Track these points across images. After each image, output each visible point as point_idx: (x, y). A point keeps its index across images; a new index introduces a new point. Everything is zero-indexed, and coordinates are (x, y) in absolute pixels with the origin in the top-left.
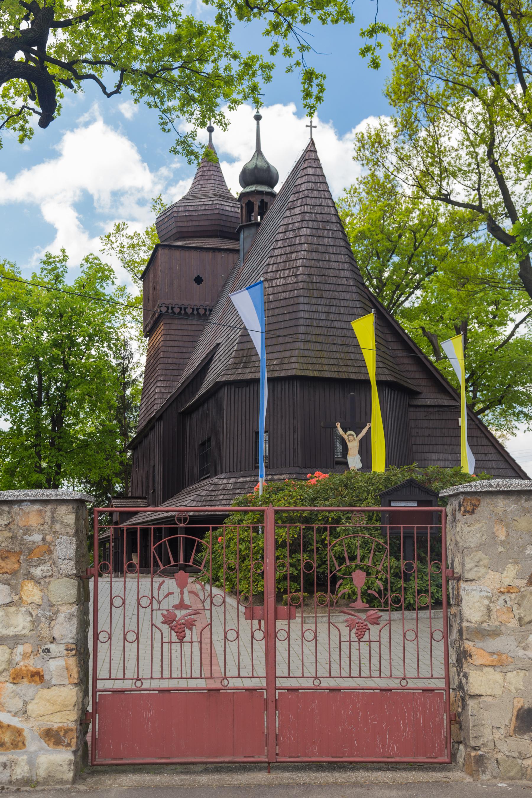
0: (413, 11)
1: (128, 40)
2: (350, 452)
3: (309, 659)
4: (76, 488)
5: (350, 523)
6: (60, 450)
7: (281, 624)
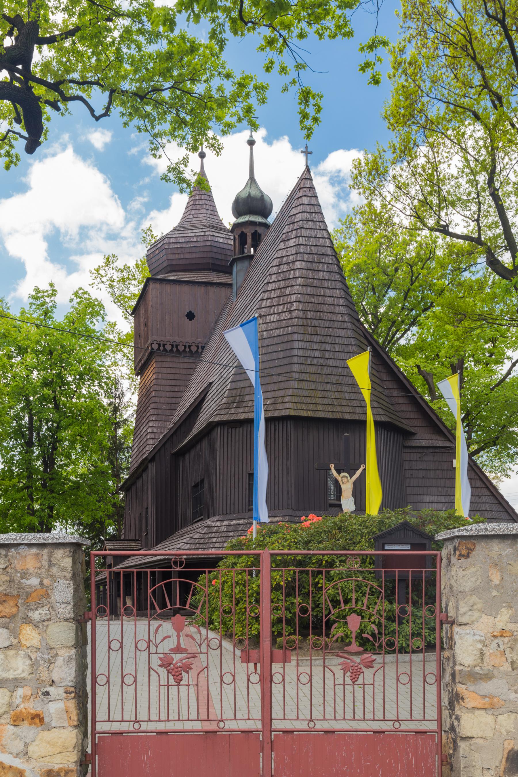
0: (414, 26)
1: (117, 58)
2: (344, 494)
3: (304, 701)
4: (68, 531)
5: (344, 566)
6: (52, 492)
7: (277, 668)
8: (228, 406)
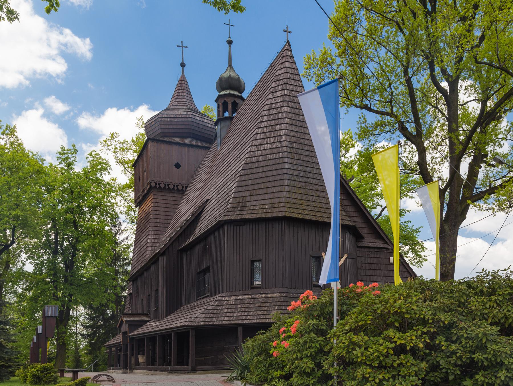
6: (71, 284)
8: (234, 209)
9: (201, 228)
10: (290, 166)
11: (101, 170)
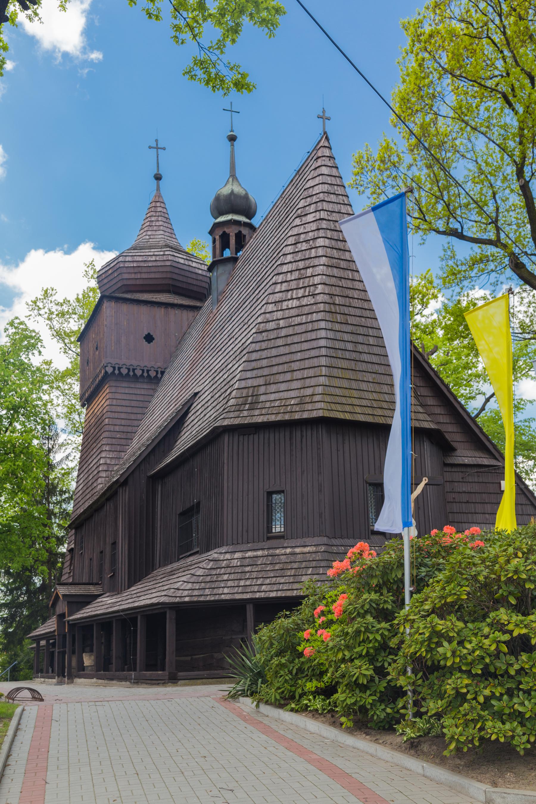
8: (239, 408)
9: (186, 439)
10: (330, 335)
11: (28, 349)
